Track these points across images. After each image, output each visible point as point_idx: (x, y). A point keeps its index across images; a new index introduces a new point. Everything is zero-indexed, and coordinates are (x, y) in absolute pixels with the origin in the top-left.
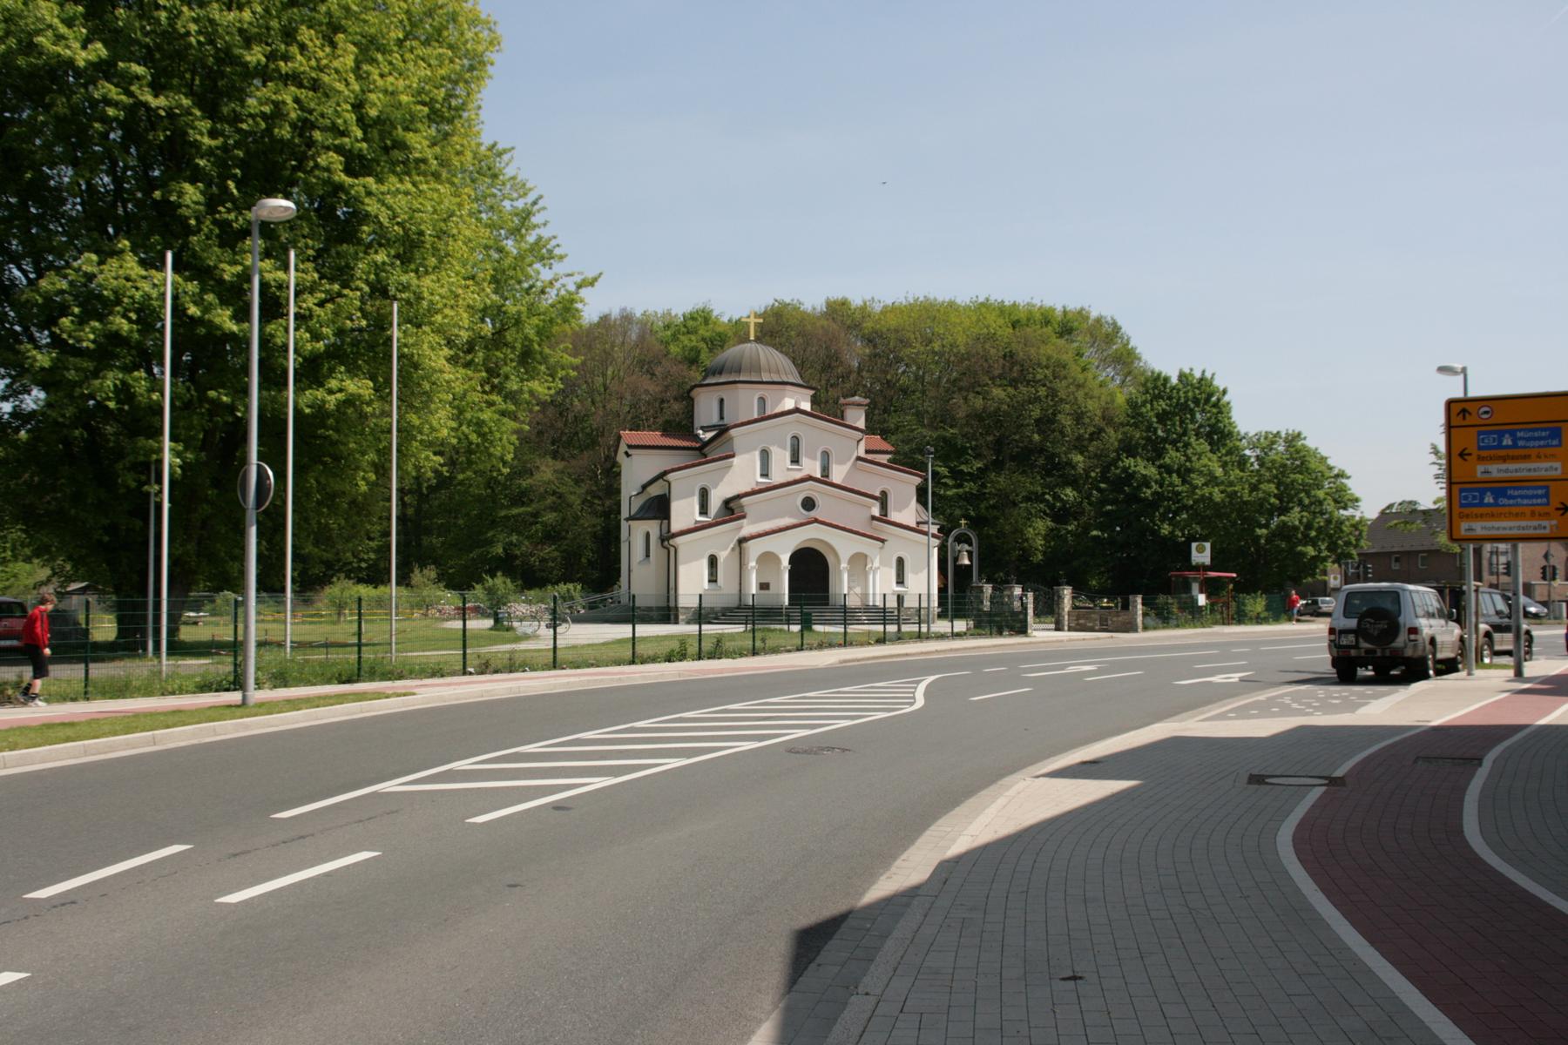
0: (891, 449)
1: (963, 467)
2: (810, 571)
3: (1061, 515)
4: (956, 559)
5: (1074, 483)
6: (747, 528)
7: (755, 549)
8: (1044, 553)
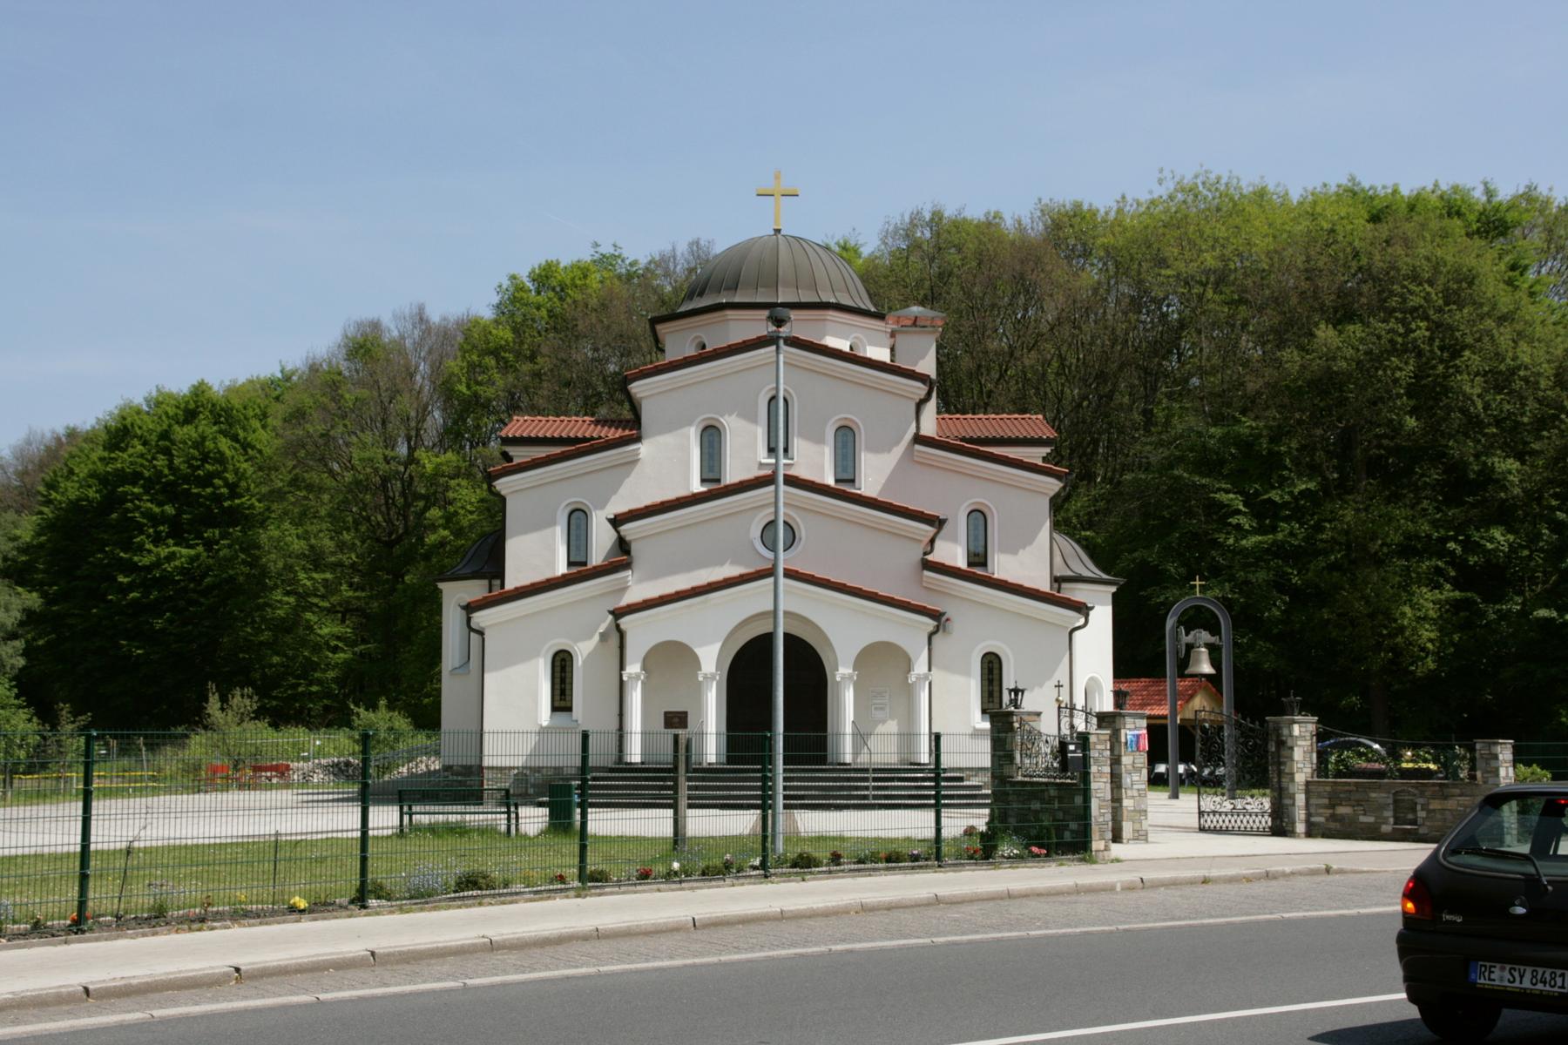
0: (1048, 433)
1: (1275, 495)
2: (779, 694)
3: (1489, 578)
5: (1504, 515)
6: (637, 588)
7: (643, 633)
8: (1440, 660)
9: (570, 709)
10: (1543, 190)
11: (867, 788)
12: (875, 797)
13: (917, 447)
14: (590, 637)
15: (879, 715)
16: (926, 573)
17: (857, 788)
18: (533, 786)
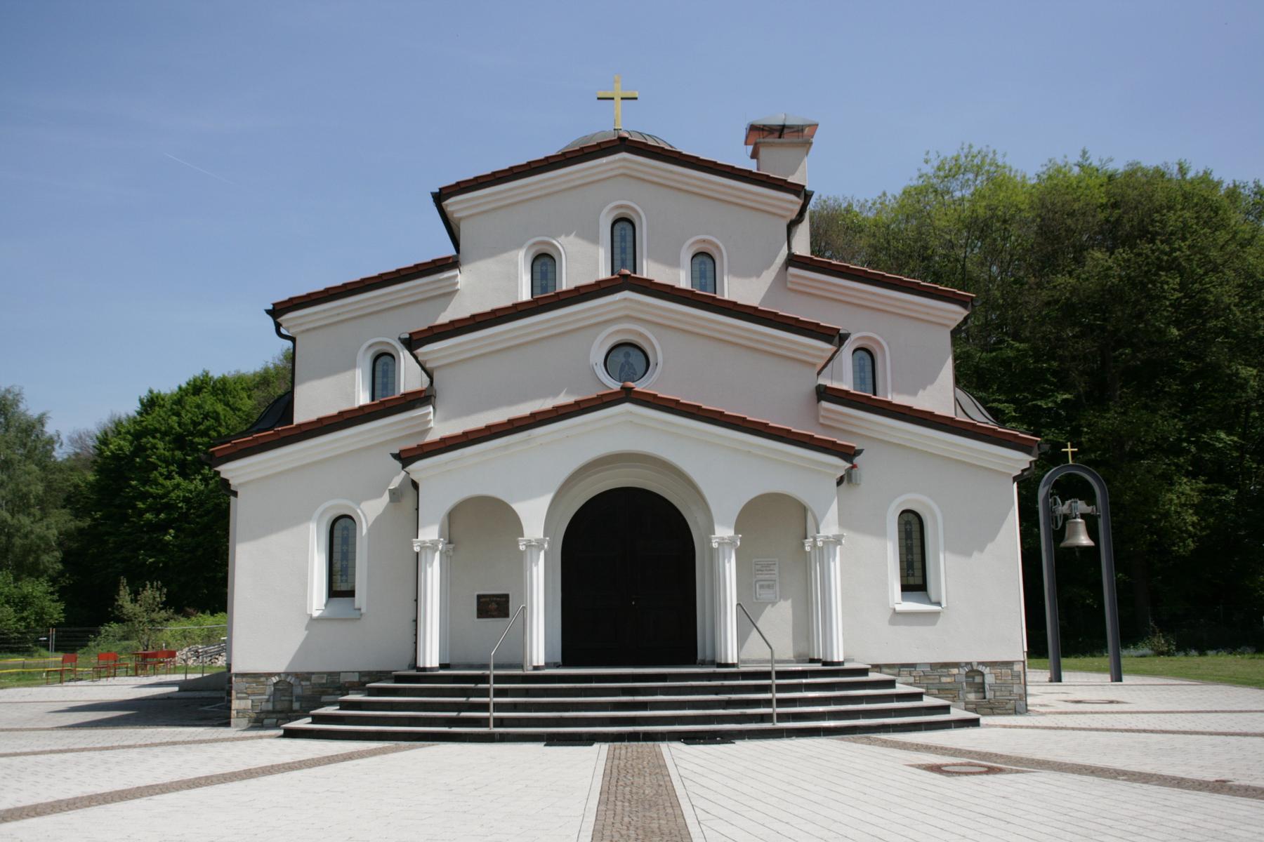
4: (1059, 535)
9: (351, 594)
10: (1216, 177)
11: (768, 703)
12: (782, 717)
13: (792, 270)
14: (380, 496)
15: (764, 594)
16: (824, 404)
17: (757, 703)
18: (299, 698)
